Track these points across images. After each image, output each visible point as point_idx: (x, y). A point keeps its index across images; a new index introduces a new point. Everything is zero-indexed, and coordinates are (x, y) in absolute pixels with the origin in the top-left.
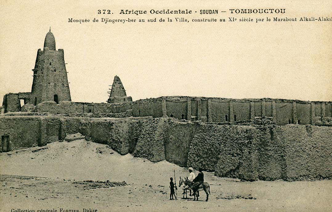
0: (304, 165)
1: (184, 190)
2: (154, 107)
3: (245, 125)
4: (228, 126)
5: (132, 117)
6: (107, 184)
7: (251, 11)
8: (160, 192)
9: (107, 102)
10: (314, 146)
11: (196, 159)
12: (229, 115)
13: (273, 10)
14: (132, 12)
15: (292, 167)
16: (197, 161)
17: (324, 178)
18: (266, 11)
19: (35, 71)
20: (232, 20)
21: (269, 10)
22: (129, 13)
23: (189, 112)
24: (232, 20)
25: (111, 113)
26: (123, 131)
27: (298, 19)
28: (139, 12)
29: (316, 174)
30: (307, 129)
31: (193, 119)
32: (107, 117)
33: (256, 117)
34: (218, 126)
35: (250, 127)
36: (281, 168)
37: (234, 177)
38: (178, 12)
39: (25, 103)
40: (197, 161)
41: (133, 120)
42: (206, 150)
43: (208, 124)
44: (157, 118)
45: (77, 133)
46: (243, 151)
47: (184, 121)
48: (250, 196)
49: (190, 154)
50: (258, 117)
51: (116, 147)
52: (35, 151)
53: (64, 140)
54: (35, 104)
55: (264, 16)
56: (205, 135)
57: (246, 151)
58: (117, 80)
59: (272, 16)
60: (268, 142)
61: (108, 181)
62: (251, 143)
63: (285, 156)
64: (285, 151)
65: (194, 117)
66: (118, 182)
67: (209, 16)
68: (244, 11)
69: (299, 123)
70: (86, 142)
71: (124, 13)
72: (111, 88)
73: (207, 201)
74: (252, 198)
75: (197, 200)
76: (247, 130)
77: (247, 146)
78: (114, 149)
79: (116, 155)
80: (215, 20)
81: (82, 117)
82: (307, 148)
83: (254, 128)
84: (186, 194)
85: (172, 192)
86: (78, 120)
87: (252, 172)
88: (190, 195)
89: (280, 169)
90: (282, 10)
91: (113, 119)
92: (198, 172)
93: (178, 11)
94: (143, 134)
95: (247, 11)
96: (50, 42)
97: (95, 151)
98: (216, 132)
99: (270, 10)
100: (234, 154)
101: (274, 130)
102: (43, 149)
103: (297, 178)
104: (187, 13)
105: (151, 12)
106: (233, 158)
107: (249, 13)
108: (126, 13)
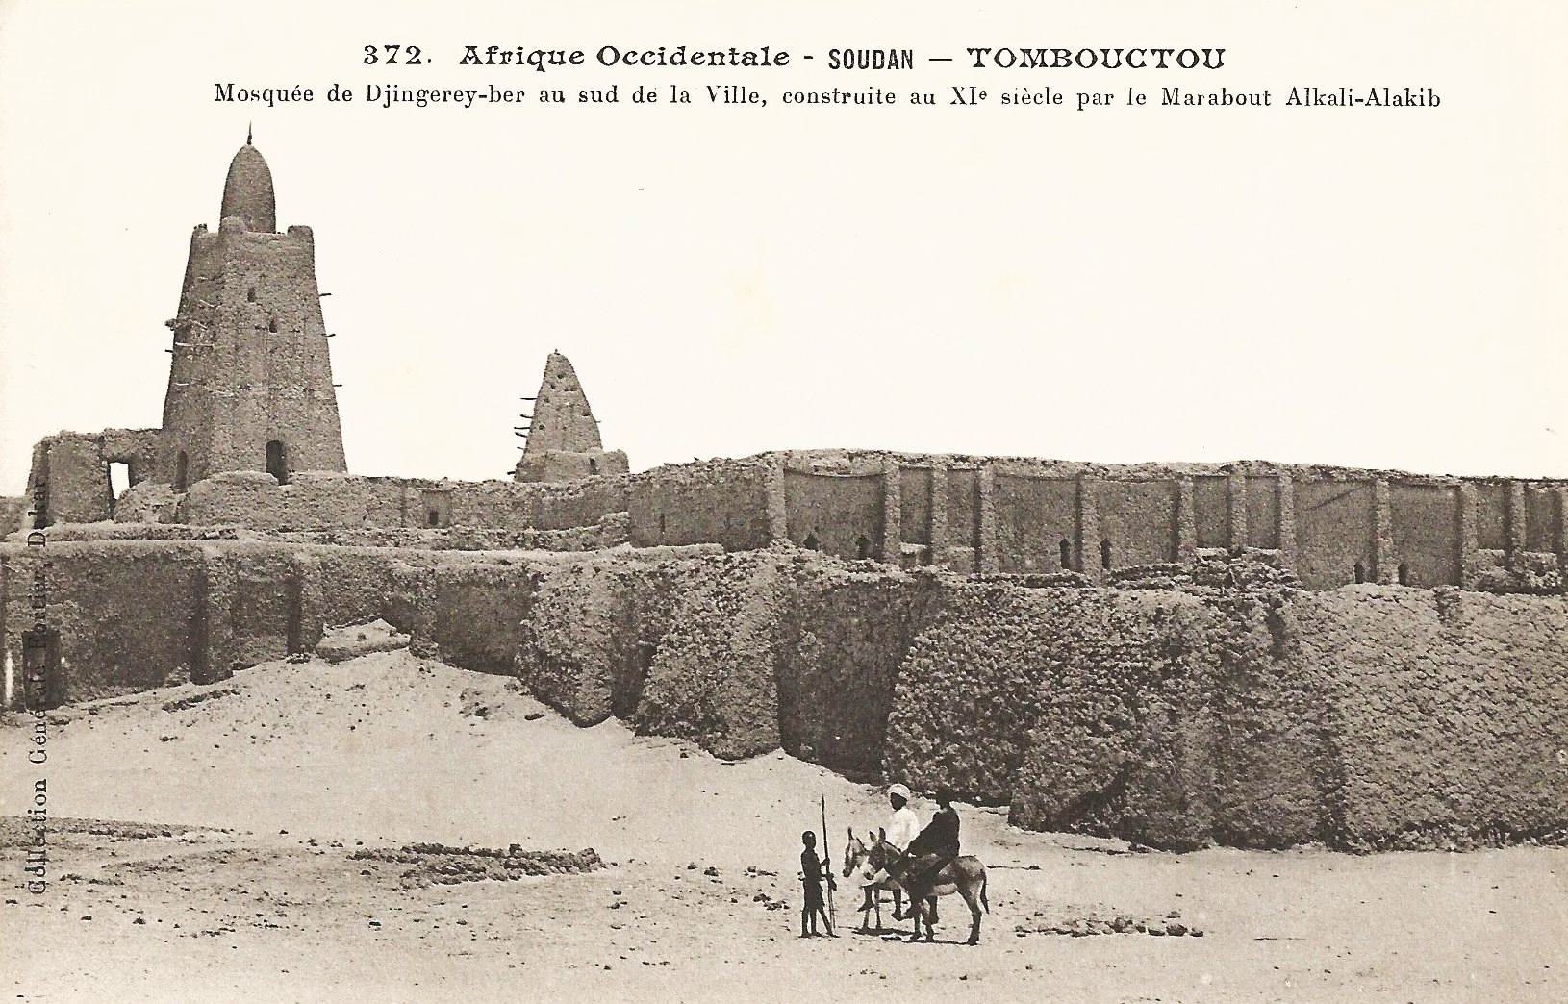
0: (1424, 776)
1: (868, 889)
2: (724, 505)
3: (1153, 587)
4: (1075, 594)
5: (627, 547)
6: (513, 861)
7: (1064, 58)
8: (756, 899)
9: (510, 479)
10: (1475, 686)
11: (926, 745)
12: (1079, 535)
13: (988, 51)
14: (515, 58)
15: (1373, 785)
16: (929, 756)
17: (1517, 838)
18: (1136, 59)
19: (180, 330)
20: (967, 98)
21: (1148, 53)
22: (504, 62)
23: (892, 528)
24: (966, 96)
25: (531, 531)
26: (584, 612)
27: (1279, 97)
28: (546, 58)
29: (1480, 819)
30: (1441, 609)
31: (907, 559)
32: (511, 548)
33: (1202, 552)
34: (1028, 591)
35: (1176, 596)
36: (1320, 788)
37: (1101, 833)
38: (727, 59)
39: (132, 482)
40: (929, 756)
41: (634, 564)
42: (971, 705)
43: (980, 580)
44: (745, 554)
45: (372, 620)
46: (1143, 710)
47: (870, 569)
48: (1173, 922)
49: (897, 720)
50: (1211, 551)
51: (552, 689)
52: (180, 705)
53: (314, 656)
54: (181, 485)
55: (1116, 81)
56: (964, 632)
57: (1155, 705)
58: (559, 370)
59: (1151, 80)
60: (1260, 668)
61: (513, 848)
62: (1179, 673)
63: (1336, 735)
64: (1337, 710)
65: (915, 548)
66: (559, 854)
67: (855, 80)
68: (1033, 59)
69: (1402, 582)
70: (413, 663)
71: (478, 62)
72: (529, 408)
73: (973, 941)
74: (1179, 931)
75: (930, 939)
76: (1160, 611)
77: (1160, 686)
78: (543, 698)
79: (555, 729)
80: (890, 98)
81: (397, 545)
82: (1440, 697)
83: (1194, 600)
84: (878, 909)
85: (813, 902)
86: (380, 567)
87: (1183, 806)
88: (897, 915)
89: (1310, 790)
90: (1106, 52)
91: (538, 558)
92: (930, 808)
93: (727, 52)
94: (677, 629)
95: (1049, 58)
96: (249, 188)
97: (457, 705)
98: (1016, 619)
99: (1153, 51)
100: (1102, 724)
101: (1288, 611)
102: (216, 695)
103: (1392, 839)
104: (766, 63)
105: (600, 56)
106: (1097, 740)
107: (1056, 65)
108: (490, 62)
